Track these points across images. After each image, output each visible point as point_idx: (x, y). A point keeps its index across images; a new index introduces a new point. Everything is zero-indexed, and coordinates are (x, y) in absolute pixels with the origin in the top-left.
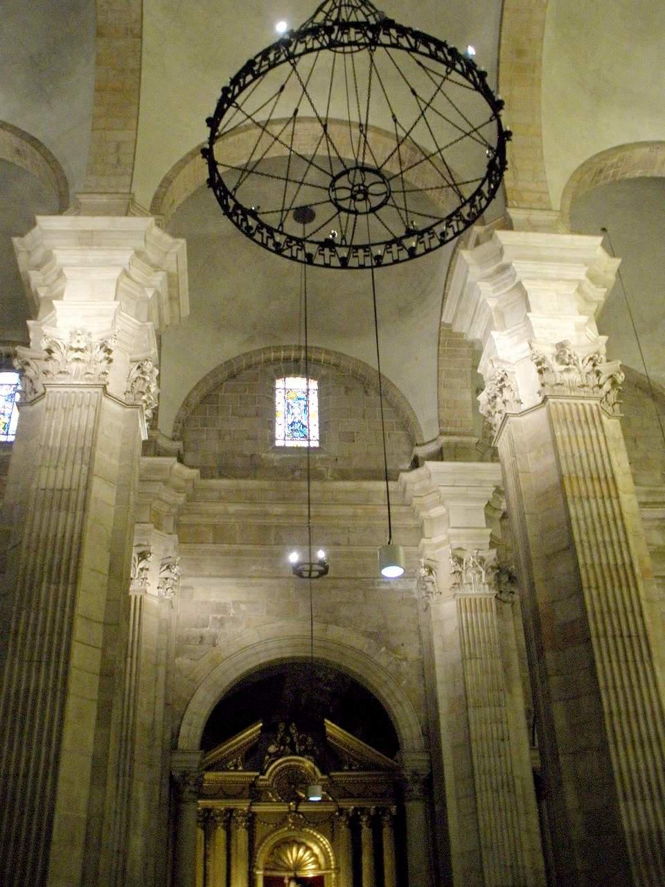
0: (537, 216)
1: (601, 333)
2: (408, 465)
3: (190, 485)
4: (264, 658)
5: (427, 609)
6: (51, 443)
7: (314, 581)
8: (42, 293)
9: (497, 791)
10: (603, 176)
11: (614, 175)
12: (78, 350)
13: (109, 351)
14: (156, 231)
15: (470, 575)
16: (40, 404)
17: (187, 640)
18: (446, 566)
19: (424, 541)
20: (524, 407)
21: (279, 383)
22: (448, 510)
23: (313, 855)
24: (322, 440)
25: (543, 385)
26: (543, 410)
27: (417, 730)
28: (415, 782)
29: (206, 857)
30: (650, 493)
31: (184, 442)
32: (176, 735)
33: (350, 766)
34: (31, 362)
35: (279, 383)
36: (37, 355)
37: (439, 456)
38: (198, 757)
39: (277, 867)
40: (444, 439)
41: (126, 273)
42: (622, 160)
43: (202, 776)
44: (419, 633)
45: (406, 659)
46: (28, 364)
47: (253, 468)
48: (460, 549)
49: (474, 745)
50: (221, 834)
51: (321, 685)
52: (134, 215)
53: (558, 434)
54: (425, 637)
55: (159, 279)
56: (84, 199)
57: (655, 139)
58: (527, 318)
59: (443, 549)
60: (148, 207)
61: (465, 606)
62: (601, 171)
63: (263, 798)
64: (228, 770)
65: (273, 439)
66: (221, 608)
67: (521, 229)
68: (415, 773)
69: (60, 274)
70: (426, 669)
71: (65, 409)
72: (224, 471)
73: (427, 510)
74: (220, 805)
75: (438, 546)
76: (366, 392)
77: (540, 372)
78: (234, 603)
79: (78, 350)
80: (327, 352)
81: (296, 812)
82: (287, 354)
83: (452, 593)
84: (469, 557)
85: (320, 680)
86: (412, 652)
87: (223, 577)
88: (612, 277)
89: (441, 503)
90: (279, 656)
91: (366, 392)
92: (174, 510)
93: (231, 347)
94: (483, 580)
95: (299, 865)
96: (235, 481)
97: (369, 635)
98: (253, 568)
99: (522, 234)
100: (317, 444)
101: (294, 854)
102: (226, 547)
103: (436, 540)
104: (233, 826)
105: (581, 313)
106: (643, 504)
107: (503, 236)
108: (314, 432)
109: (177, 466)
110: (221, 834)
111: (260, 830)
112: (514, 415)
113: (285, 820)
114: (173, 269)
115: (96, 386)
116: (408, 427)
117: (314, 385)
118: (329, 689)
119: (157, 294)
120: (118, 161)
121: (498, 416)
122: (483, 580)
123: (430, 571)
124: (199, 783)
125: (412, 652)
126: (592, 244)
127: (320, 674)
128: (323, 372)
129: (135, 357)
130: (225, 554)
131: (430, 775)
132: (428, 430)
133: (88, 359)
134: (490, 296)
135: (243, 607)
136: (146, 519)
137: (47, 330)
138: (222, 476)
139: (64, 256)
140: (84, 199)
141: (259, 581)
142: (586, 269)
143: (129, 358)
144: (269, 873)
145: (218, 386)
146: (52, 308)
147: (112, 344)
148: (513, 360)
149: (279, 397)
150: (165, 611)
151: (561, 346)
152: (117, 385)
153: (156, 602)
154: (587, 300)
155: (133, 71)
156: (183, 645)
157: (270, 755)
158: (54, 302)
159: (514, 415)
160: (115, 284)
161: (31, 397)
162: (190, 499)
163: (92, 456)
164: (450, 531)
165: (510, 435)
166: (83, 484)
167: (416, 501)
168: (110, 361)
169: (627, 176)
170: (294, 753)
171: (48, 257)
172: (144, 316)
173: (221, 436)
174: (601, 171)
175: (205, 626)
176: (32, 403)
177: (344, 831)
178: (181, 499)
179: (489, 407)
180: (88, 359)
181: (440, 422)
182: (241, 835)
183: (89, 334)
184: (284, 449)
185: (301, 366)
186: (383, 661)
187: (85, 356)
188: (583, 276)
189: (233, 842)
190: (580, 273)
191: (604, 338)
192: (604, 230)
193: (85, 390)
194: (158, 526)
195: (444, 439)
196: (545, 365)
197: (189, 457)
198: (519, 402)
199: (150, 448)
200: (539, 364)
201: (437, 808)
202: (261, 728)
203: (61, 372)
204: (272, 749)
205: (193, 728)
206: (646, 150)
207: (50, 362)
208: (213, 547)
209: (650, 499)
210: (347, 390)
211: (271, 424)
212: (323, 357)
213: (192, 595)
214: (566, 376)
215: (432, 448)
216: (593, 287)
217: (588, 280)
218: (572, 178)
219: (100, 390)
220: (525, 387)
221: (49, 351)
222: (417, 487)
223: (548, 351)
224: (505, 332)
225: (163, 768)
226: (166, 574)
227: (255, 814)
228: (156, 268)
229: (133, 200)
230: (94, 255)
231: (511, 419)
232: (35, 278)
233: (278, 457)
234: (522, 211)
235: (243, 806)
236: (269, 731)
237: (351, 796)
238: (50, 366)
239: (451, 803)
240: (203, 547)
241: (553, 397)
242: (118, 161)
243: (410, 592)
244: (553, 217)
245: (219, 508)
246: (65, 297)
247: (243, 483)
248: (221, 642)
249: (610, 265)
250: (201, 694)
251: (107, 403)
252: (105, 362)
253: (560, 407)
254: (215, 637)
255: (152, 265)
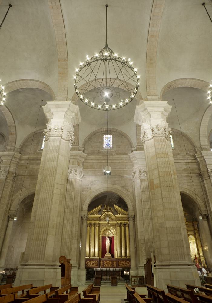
0: (154, 97)
1: (167, 122)
2: (130, 152)
3: (85, 157)
4: (100, 192)
5: (134, 181)
6: (50, 148)
7: (108, 176)
8: (49, 118)
9: (148, 219)
10: (171, 87)
11: (174, 87)
12: (56, 129)
13: (62, 129)
14: (72, 104)
15: (143, 174)
16: (49, 140)
17: (85, 188)
18: (137, 173)
19: (134, 167)
20: (149, 139)
21: (104, 136)
22: (138, 161)
23: (112, 232)
24: (113, 147)
25: (153, 134)
26: (153, 139)
27: (132, 207)
28: (131, 217)
29: (90, 232)
30: (183, 157)
31: (84, 148)
32: (82, 208)
33: (119, 214)
34: (47, 132)
35: (104, 136)
36: (48, 131)
37: (137, 150)
38: (87, 212)
39: (105, 234)
40: (137, 147)
41: (66, 113)
42: (175, 83)
43: (88, 216)
44: (132, 186)
45: (129, 192)
46: (46, 132)
47: (99, 153)
48: (141, 169)
49: (143, 210)
50: (93, 228)
51: (114, 197)
52: (68, 101)
53: (156, 144)
54: (133, 187)
55: (73, 114)
56: (57, 98)
57: (183, 78)
58: (150, 120)
59: (137, 169)
60: (71, 99)
61: (142, 181)
62: (170, 86)
63: (102, 221)
64: (95, 215)
65: (103, 147)
66: (92, 182)
67: (150, 100)
68: (131, 215)
69: (52, 114)
70: (133, 194)
71: (53, 141)
72: (93, 153)
73: (134, 161)
74: (93, 222)
75: (136, 169)
76: (122, 137)
77: (152, 131)
78: (95, 180)
79: (56, 129)
80: (114, 129)
81: (108, 223)
82: (106, 130)
83: (139, 178)
84: (142, 171)
85: (113, 196)
86: (131, 190)
87: (92, 175)
88: (170, 110)
89: (137, 159)
90: (101, 192)
91: (122, 137)
92: (82, 162)
93: (94, 129)
94: (145, 175)
95: (109, 234)
96: (95, 156)
97: (122, 187)
98: (99, 173)
99: (150, 101)
100: (112, 148)
101: (108, 232)
102: (93, 169)
103: (136, 167)
104: (95, 226)
105: (162, 118)
106: (174, 159)
107: (146, 102)
108: (111, 146)
109: (83, 153)
110: (93, 228)
111: (101, 227)
112: (147, 140)
113: (106, 225)
114: (76, 112)
115: (60, 137)
116: (131, 144)
117: (111, 136)
118: (115, 198)
119: (73, 117)
120: (64, 89)
121: (144, 141)
122: (145, 175)
123: (134, 174)
124: (87, 218)
125: (131, 190)
126: (165, 103)
127: (114, 195)
128: (113, 133)
129: (69, 130)
130: (93, 171)
131: (134, 216)
132: (135, 145)
133: (58, 131)
134: (142, 115)
135: (96, 181)
136: (76, 164)
137: (50, 125)
138: (92, 155)
139: (53, 110)
140: (57, 98)
141: (100, 176)
142: (164, 108)
143: (67, 131)
144: (103, 236)
145: (91, 136)
146: (51, 121)
147: (63, 128)
148: (147, 129)
149: (104, 139)
150: (80, 182)
151: (157, 125)
152: (64, 136)
153: (78, 181)
154: (164, 115)
155: (66, 69)
156: (83, 190)
157: (103, 212)
158: (51, 120)
159: (147, 140)
160: (64, 116)
161: (47, 139)
162: (86, 159)
163: (59, 151)
164: (139, 165)
165: (146, 145)
166: (57, 156)
167: (132, 159)
168: (63, 131)
169: (177, 87)
170: (108, 211)
171: (50, 110)
172: (70, 122)
173: (92, 147)
174: (170, 86)
175: (89, 185)
176: (47, 140)
177: (118, 228)
178: (83, 160)
179: (142, 139)
180: (58, 131)
181: (137, 143)
182: (97, 228)
183: (58, 126)
184: (105, 149)
185: (108, 132)
186: (125, 192)
187: (57, 131)
188: (163, 110)
189: (96, 229)
190: (162, 109)
191: (168, 123)
192: (173, 100)
193: (58, 138)
194: (79, 165)
195: (137, 147)
196: (153, 130)
197: (86, 151)
198: (148, 138)
199: (72, 149)
200: (152, 129)
201: (136, 223)
202: (101, 206)
203: (52, 134)
204: (104, 210)
205: (86, 207)
206: (181, 81)
207: (50, 132)
208: (90, 169)
209: (183, 158)
210: (118, 137)
211: (102, 144)
212: (113, 130)
213: (86, 179)
214: (158, 132)
215: (135, 148)
216: (166, 112)
217: (164, 111)
218: (163, 88)
219: (60, 137)
220: (149, 134)
221: (50, 130)
222: (132, 156)
223: (154, 127)
224: (146, 123)
225: (79, 214)
226: (81, 175)
227: (100, 224)
228: (73, 112)
229: (67, 98)
230: (59, 109)
231: (146, 141)
232: (47, 115)
233: (104, 151)
234: (150, 96)
235: (97, 222)
236: (103, 206)
237: (120, 220)
238: (50, 133)
239: (138, 222)
240: (88, 169)
241: (155, 136)
242: (64, 89)
243: (131, 178)
244: (157, 97)
245: (91, 161)
246: (53, 118)
247: (96, 156)
248: (92, 189)
249: (170, 107)
250: (88, 199)
251: (62, 140)
252: (61, 132)
253: (159, 138)
254: (91, 187)
255: (72, 111)
